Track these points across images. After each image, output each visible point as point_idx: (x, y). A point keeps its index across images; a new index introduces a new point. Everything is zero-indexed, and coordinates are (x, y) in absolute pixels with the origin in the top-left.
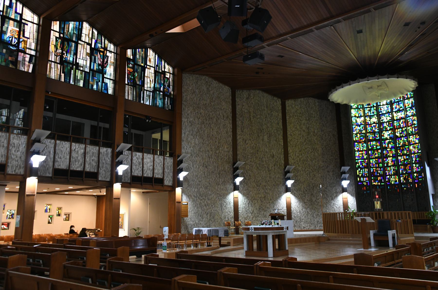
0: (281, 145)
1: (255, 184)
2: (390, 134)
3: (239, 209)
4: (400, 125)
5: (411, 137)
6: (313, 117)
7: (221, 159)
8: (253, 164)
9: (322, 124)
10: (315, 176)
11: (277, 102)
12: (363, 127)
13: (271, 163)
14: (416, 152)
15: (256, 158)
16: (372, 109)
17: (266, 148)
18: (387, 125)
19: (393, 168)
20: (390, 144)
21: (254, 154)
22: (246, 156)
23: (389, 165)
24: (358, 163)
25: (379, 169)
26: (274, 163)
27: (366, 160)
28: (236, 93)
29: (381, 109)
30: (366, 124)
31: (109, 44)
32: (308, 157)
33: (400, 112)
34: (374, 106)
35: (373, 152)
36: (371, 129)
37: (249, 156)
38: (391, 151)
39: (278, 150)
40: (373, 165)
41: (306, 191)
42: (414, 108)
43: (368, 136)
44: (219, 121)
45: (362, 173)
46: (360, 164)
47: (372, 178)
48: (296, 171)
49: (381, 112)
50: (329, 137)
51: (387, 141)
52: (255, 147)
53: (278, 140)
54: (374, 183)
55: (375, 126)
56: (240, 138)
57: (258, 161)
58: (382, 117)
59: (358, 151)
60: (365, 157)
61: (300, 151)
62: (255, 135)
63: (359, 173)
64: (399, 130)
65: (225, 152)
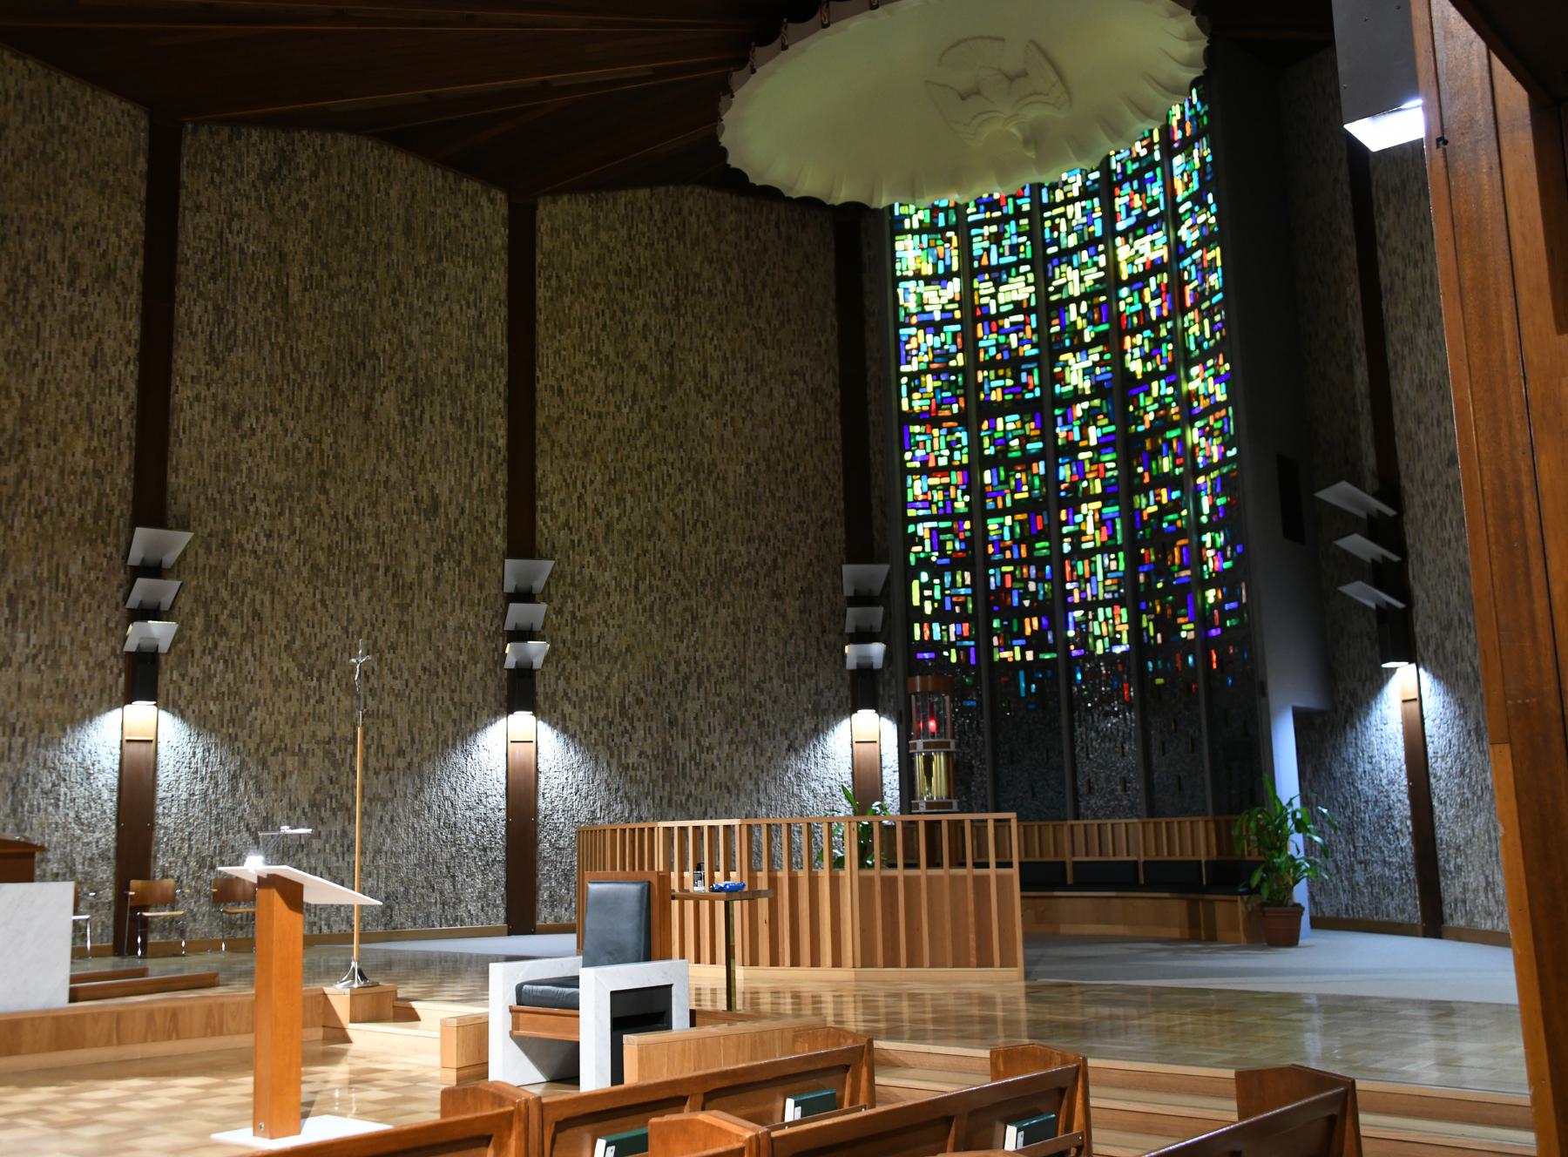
0: (491, 446)
1: (288, 664)
2: (1095, 364)
3: (160, 810)
4: (1146, 307)
5: (1195, 371)
6: (700, 292)
7: (38, 517)
8: (286, 547)
9: (754, 328)
10: (694, 618)
11: (479, 206)
12: (955, 334)
13: (416, 543)
14: (1215, 459)
15: (312, 514)
16: (1011, 228)
17: (383, 462)
18: (1083, 316)
19: (1106, 561)
20: (1095, 424)
21: (297, 494)
22: (233, 504)
23: (1084, 546)
24: (916, 540)
25: (1033, 571)
26: (433, 548)
27: (967, 525)
28: (188, 140)
29: (1055, 227)
30: (972, 314)
31: (14, 61)
32: (657, 512)
33: (1145, 234)
34: (1018, 214)
35: (1002, 473)
36: (998, 345)
37: (258, 503)
38: (1099, 462)
39: (472, 476)
40: (1002, 551)
41: (639, 701)
42: (1210, 198)
43: (980, 387)
44: (34, 292)
45: (937, 595)
46: (927, 543)
47: (996, 624)
48: (578, 597)
49: (1056, 242)
50: (793, 403)
51: (1079, 409)
52: (309, 454)
53: (470, 416)
54: (1005, 654)
55: (1018, 328)
56: (197, 398)
57: (325, 533)
58: (1057, 271)
59: (926, 470)
60: (960, 506)
61: (612, 482)
62: (312, 388)
63: (923, 598)
64: (1138, 339)
65: (73, 472)
